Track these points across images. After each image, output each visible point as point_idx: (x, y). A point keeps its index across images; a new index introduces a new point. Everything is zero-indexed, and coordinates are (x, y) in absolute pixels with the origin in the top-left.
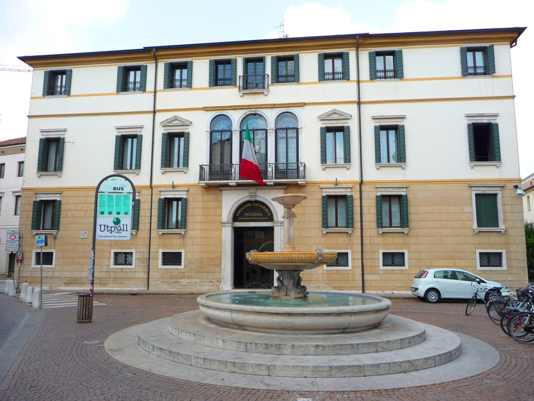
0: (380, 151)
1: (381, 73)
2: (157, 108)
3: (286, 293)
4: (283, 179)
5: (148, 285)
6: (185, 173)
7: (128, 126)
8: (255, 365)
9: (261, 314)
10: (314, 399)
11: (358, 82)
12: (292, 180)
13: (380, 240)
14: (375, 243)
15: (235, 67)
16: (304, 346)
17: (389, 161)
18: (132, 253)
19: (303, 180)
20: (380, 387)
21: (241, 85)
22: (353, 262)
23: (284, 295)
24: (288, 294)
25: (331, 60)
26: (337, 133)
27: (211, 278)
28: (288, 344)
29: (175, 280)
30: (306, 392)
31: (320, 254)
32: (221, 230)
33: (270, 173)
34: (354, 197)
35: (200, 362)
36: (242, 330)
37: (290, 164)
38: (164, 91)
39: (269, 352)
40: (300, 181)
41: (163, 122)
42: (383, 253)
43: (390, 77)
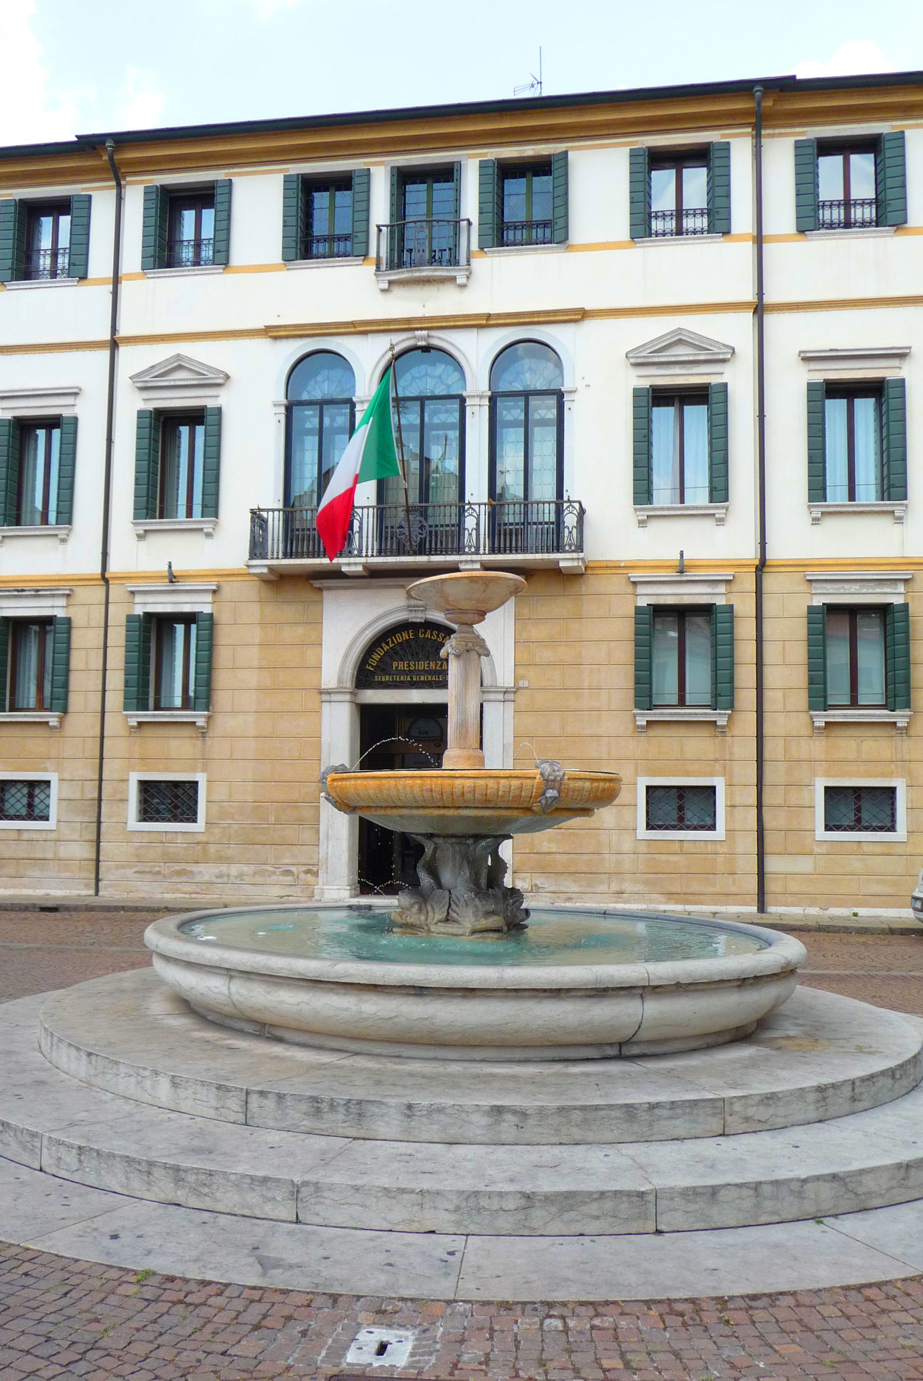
0: (824, 462)
1: (835, 211)
2: (124, 330)
3: (448, 913)
4: (511, 552)
5: (98, 880)
6: (209, 535)
7: (33, 390)
8: (249, 1181)
9: (322, 985)
10: (427, 1335)
11: (759, 240)
12: (539, 556)
13: (817, 747)
14: (803, 757)
15: (363, 196)
16: (448, 1111)
17: (852, 496)
18: (48, 783)
19: (575, 555)
20: (704, 1288)
21: (384, 254)
22: (729, 817)
23: (440, 921)
24: (454, 915)
25: (673, 172)
26: (687, 408)
27: (287, 861)
28: (392, 1101)
29: (177, 867)
30: (400, 1304)
31: (551, 778)
32: (319, 712)
33: (470, 534)
34: (739, 609)
35: (68, 1160)
36: (268, 1038)
37: (535, 505)
38: (143, 276)
39: (323, 1126)
40: (566, 559)
41: (138, 375)
42: (827, 789)
43: (864, 224)
